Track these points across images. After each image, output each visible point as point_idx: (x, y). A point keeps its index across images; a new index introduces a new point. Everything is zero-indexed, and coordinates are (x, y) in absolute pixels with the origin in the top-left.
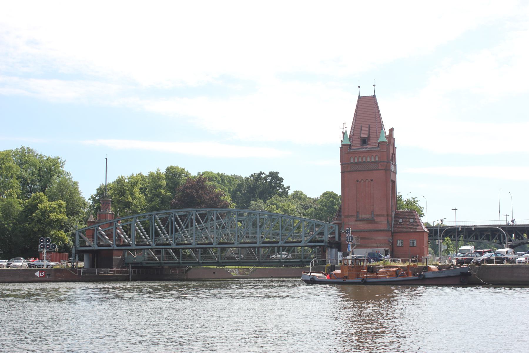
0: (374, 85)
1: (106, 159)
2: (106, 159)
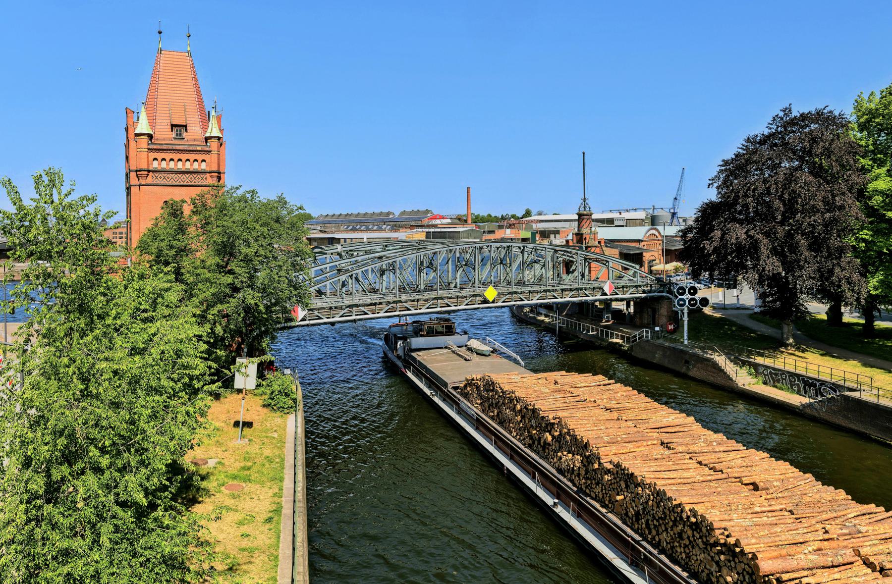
0: (160, 33)
1: (584, 153)
2: (584, 153)
